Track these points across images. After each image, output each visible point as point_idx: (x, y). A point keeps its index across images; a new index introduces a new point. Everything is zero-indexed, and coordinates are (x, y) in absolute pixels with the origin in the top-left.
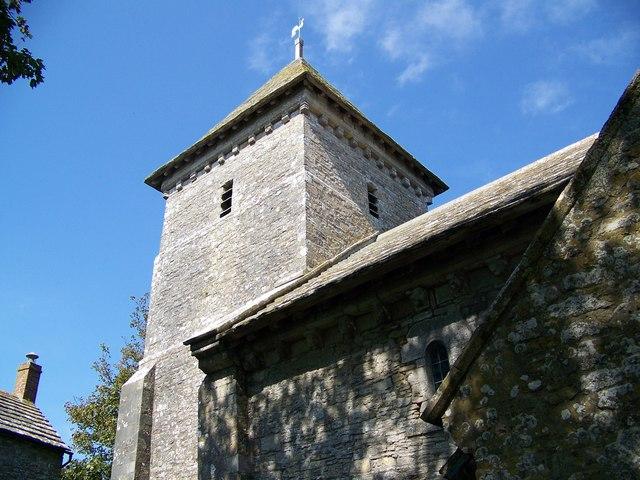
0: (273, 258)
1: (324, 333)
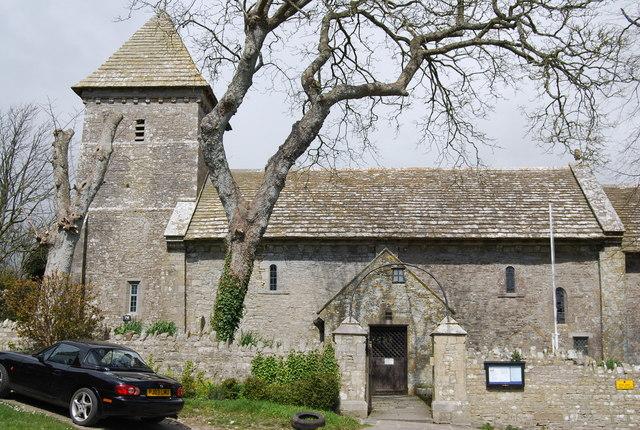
0: (175, 183)
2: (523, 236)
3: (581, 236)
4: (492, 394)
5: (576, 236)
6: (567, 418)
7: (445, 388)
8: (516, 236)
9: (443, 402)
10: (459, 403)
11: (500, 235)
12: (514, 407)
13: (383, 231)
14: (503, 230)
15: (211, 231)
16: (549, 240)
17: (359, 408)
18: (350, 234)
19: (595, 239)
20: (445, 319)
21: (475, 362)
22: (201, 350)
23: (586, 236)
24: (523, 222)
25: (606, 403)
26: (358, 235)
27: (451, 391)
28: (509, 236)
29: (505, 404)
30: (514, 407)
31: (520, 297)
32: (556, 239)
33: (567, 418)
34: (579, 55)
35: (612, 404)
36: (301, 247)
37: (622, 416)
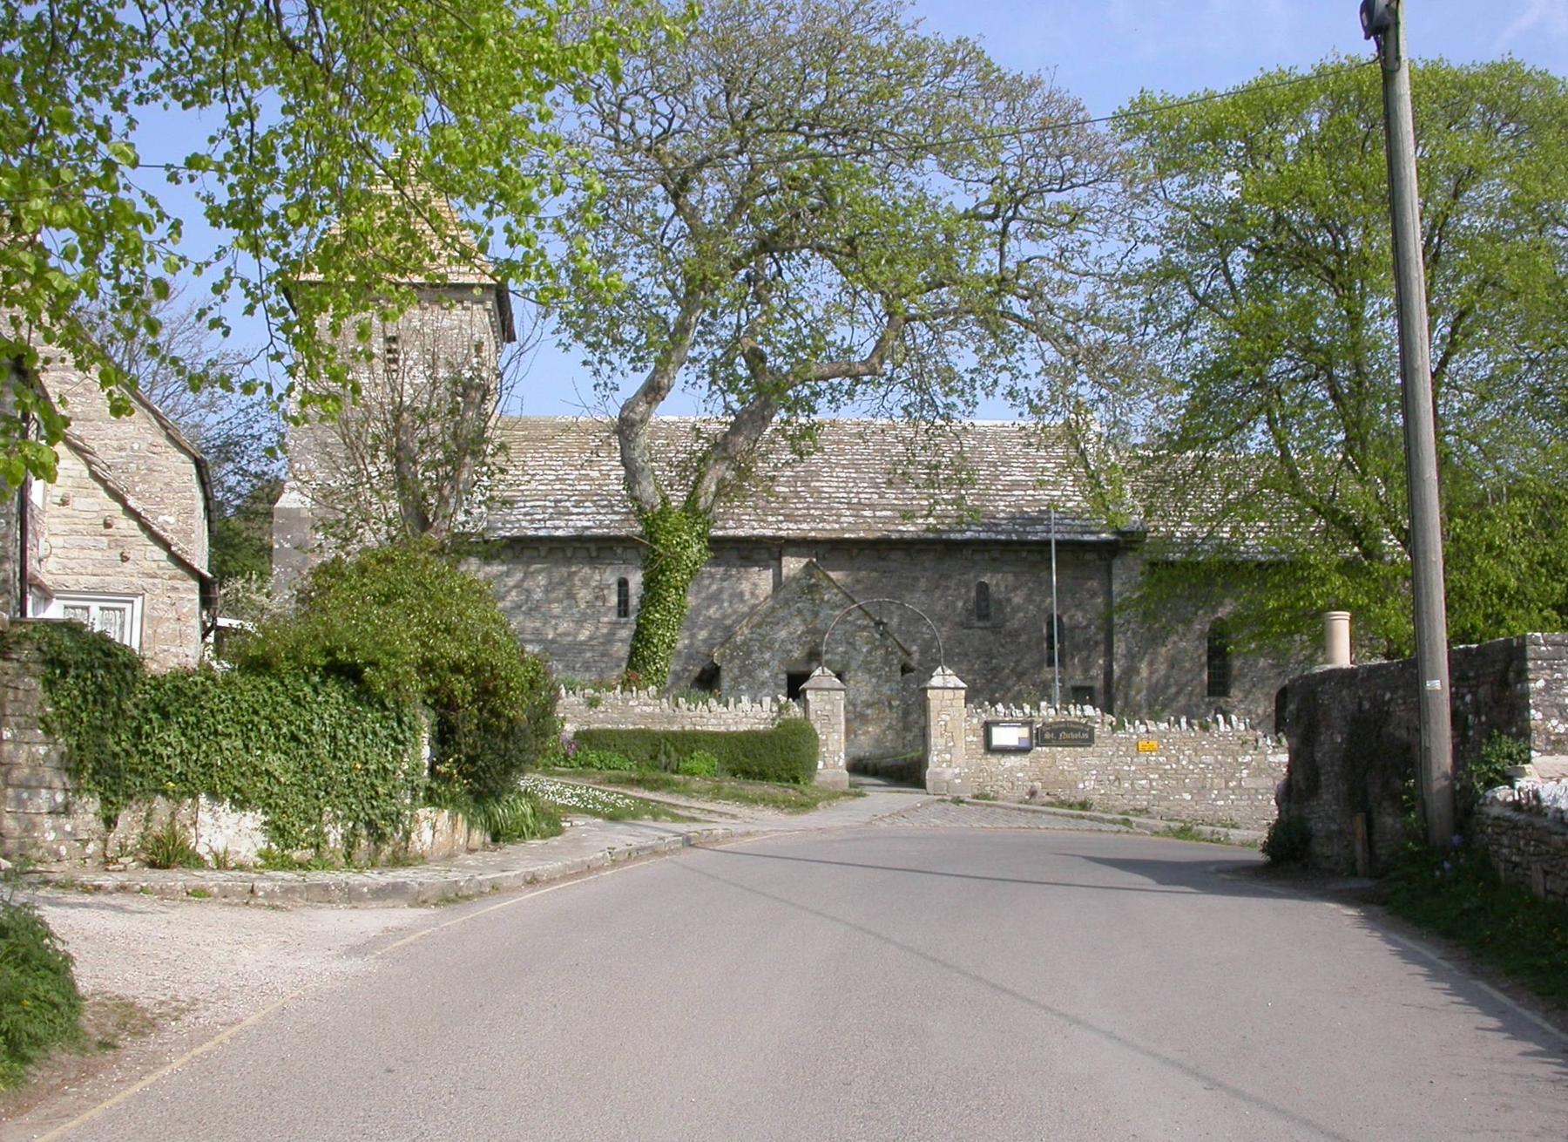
1: (551, 550)
2: (1003, 537)
3: (1087, 537)
4: (993, 759)
5: (1079, 537)
6: (1081, 786)
7: (940, 752)
8: (993, 536)
9: (938, 770)
10: (957, 771)
11: (968, 535)
12: (1020, 775)
13: (791, 526)
14: (973, 528)
15: (524, 524)
16: (1048, 543)
17: (838, 778)
18: (741, 533)
19: (1107, 543)
20: (939, 669)
21: (975, 721)
22: (638, 710)
23: (1093, 538)
24: (1002, 515)
25: (1126, 768)
26: (755, 532)
27: (948, 756)
28: (983, 536)
29: (1011, 770)
30: (1020, 775)
31: (996, 629)
32: (1058, 543)
33: (1081, 786)
34: (169, 19)
35: (1133, 768)
36: (967, 552)
37: (1144, 782)
